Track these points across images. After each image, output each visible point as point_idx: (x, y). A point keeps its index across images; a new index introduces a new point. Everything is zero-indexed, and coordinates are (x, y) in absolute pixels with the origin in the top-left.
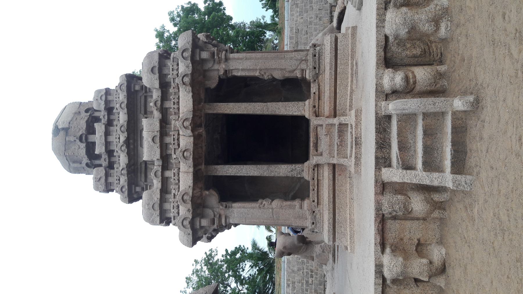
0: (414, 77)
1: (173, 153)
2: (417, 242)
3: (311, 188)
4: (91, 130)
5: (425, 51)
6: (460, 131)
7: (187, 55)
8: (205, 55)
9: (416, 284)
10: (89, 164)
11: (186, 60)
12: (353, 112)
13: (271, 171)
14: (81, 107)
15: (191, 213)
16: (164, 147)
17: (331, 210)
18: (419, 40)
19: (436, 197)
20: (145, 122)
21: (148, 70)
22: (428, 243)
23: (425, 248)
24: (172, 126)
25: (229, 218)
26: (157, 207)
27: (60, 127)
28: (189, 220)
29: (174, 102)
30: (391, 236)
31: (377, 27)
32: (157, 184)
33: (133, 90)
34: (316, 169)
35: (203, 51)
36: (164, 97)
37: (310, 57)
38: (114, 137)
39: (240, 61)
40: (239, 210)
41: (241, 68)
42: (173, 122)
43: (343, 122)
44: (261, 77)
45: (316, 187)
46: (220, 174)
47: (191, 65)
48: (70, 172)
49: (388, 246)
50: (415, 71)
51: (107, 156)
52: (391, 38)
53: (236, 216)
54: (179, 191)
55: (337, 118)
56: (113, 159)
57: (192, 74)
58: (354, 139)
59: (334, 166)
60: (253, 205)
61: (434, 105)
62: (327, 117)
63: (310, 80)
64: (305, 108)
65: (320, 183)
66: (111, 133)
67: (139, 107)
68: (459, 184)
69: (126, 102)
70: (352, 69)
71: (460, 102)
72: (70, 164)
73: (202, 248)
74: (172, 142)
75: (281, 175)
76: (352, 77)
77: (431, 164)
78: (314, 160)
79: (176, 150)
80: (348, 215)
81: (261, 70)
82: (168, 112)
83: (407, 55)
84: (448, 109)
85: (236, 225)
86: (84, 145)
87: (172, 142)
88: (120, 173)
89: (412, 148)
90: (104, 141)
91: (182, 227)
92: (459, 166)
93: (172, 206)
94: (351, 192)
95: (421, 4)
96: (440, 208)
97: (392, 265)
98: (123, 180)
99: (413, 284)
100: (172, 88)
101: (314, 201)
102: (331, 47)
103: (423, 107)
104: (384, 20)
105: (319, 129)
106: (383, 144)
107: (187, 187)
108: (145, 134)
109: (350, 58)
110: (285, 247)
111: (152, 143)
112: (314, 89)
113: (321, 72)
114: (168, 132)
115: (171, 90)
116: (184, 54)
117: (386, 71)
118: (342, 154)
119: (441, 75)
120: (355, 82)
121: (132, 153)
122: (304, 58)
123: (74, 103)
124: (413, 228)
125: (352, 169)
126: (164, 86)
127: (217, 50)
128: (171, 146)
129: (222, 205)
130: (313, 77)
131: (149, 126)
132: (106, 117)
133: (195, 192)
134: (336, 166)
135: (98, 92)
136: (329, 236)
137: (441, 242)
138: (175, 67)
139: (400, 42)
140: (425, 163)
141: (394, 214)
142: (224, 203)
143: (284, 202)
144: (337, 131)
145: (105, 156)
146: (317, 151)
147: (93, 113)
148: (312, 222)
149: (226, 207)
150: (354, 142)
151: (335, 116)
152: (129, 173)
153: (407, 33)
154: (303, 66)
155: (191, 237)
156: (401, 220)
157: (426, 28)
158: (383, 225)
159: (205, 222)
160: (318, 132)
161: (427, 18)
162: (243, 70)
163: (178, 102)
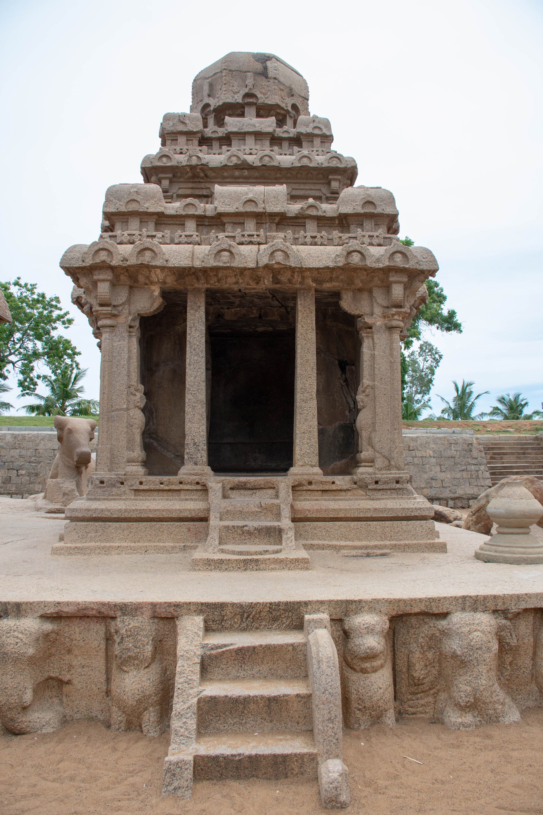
0: (375, 670)
1: (227, 234)
2: (66, 679)
3: (165, 478)
4: (263, 111)
5: (419, 685)
6: (276, 769)
7: (398, 260)
8: (398, 291)
10: (208, 110)
11: (389, 259)
12: (303, 554)
13: (194, 408)
14: (301, 99)
15: (121, 263)
16: (238, 218)
17: (127, 515)
18: (440, 673)
19: (150, 717)
20: (282, 189)
21: (369, 196)
22: (65, 700)
23: (54, 694)
24: (274, 234)
25: (112, 332)
26: (133, 207)
27: (269, 64)
28: (108, 260)
29: (315, 237)
30: (75, 631)
31: (464, 598)
32: (174, 207)
33: (330, 177)
34: (199, 487)
35: (405, 289)
36: (324, 222)
37: (394, 474)
38: (253, 147)
39: (388, 351)
40: (126, 350)
41: (376, 353)
42: (281, 235)
43: (284, 536)
44: (360, 389)
45: (167, 488)
46: (189, 316)
47: (381, 266)
48: (195, 80)
49: (56, 627)
50: (385, 669)
51: (220, 135)
52: (443, 623)
53: (115, 344)
54: (160, 243)
55: (292, 525)
56: (216, 144)
57: (366, 269)
58: (255, 557)
59: (205, 519)
60: (135, 376)
61: (330, 719)
62: (292, 506)
63: (355, 473)
64: (308, 467)
65: (175, 494)
66: (259, 142)
67: (302, 187)
68: (174, 775)
69: (311, 165)
70: (376, 547)
71: (336, 775)
72: (208, 78)
73: (61, 288)
74: (246, 233)
75: (188, 425)
76: (361, 548)
77: (213, 715)
78: (216, 483)
79: (232, 239)
80: (117, 544)
81: (373, 387)
82: (297, 228)
83: (412, 652)
84: (321, 747)
85: (99, 346)
86: (240, 100)
87: (246, 233)
88: (192, 154)
89: (242, 673)
90: (247, 121)
91: (96, 248)
92: (208, 770)
93: (133, 232)
94: (159, 550)
95: (502, 673)
97: (20, 636)
98: (181, 159)
100: (340, 235)
101: (141, 483)
102: (412, 510)
103: (325, 699)
104: (475, 610)
105: (271, 492)
106: (248, 617)
107: (167, 257)
108: (260, 188)
109: (394, 542)
110: (70, 431)
111: (244, 199)
112: (341, 481)
113: (370, 493)
114: (264, 226)
115: (336, 234)
116: (399, 255)
117: (386, 618)
118: (229, 534)
119: (377, 719)
120: (354, 552)
121: (225, 174)
122: (393, 463)
123: (307, 88)
124: (90, 673)
125: (199, 554)
126: (343, 222)
127: (406, 313)
128: (239, 230)
129: (133, 320)
130: (360, 480)
131: (274, 196)
132: (286, 135)
133: (158, 271)
135: (327, 124)
136: (81, 510)
137: (65, 721)
138: (375, 241)
139: (435, 642)
140: (213, 701)
141: (117, 639)
142: (137, 324)
143: (139, 430)
144: (269, 524)
145: (221, 132)
146: (232, 489)
147: (291, 117)
148: (105, 480)
149: (131, 327)
150: (249, 557)
151: (294, 520)
153: (454, 653)
154: (380, 462)
155: (80, 264)
156: (107, 649)
157: (463, 687)
158: (96, 617)
159: (104, 288)
160: (265, 491)
161: (482, 689)
162: (373, 356)
163: (316, 244)
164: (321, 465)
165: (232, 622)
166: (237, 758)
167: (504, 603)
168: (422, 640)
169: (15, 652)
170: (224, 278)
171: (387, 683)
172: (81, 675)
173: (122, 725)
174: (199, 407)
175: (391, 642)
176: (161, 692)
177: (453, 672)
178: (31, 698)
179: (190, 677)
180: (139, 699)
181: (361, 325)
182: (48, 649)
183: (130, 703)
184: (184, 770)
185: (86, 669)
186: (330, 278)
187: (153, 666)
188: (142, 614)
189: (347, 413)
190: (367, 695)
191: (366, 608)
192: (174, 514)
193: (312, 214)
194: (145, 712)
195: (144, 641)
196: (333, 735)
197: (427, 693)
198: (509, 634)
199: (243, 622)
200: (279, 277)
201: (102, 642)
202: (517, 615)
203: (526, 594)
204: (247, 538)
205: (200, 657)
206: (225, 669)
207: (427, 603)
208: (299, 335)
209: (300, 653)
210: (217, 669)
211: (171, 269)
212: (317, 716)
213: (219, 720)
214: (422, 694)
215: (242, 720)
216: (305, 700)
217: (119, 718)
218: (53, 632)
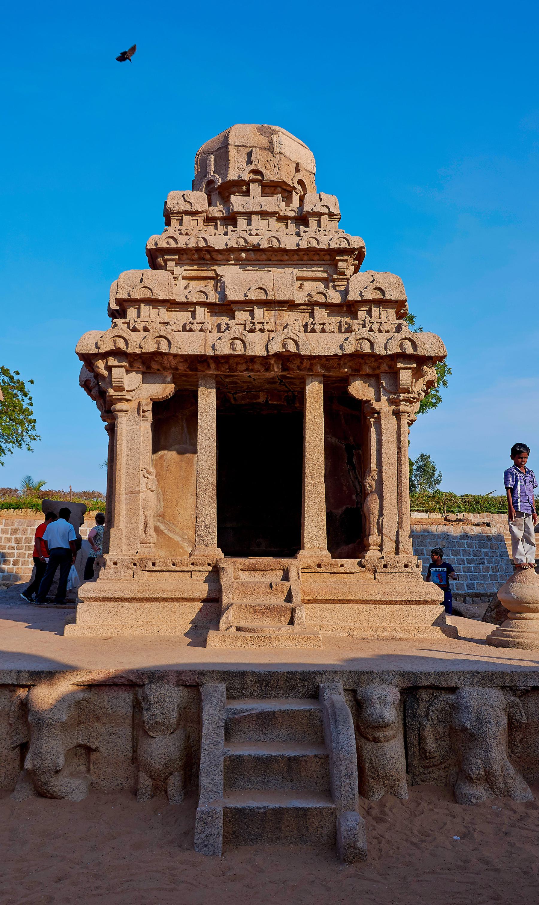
2: (94, 747)
4: (271, 188)
5: (430, 758)
9: (17, 746)
19: (175, 782)
22: (92, 767)
49: (86, 695)
57: (373, 356)
96: (156, 788)
99: (20, 739)
112: (351, 564)
133: (171, 358)
134: (215, 604)
142: (150, 407)
152: (198, 250)
158: (124, 685)
164: (329, 549)
165: (252, 690)
166: (262, 811)
167: (512, 680)
168: (432, 713)
169: (50, 718)
170: (235, 365)
171: (399, 753)
172: (108, 743)
173: (148, 789)
174: (210, 489)
175: (402, 715)
176: (185, 758)
177: (463, 746)
178: (63, 763)
179: (215, 740)
180: (166, 764)
181: (369, 410)
182: (79, 716)
183: (157, 767)
184: (215, 818)
185: (113, 737)
186: (338, 364)
187: (178, 732)
188: (168, 682)
189: (354, 497)
190: (380, 763)
191: (378, 679)
192: (186, 594)
193: (320, 301)
194: (171, 776)
195: (170, 708)
196: (350, 790)
197: (439, 767)
198: (518, 712)
199: (262, 690)
200: (288, 364)
201: (129, 710)
202: (526, 693)
203: (534, 672)
204: (259, 617)
205: (224, 721)
206: (246, 733)
207: (436, 677)
208: (307, 420)
209: (316, 718)
210: (239, 733)
211: (182, 356)
212: (335, 772)
213: (243, 778)
214: (433, 768)
215: (265, 779)
216: (323, 761)
217: (146, 783)
218: (84, 699)
